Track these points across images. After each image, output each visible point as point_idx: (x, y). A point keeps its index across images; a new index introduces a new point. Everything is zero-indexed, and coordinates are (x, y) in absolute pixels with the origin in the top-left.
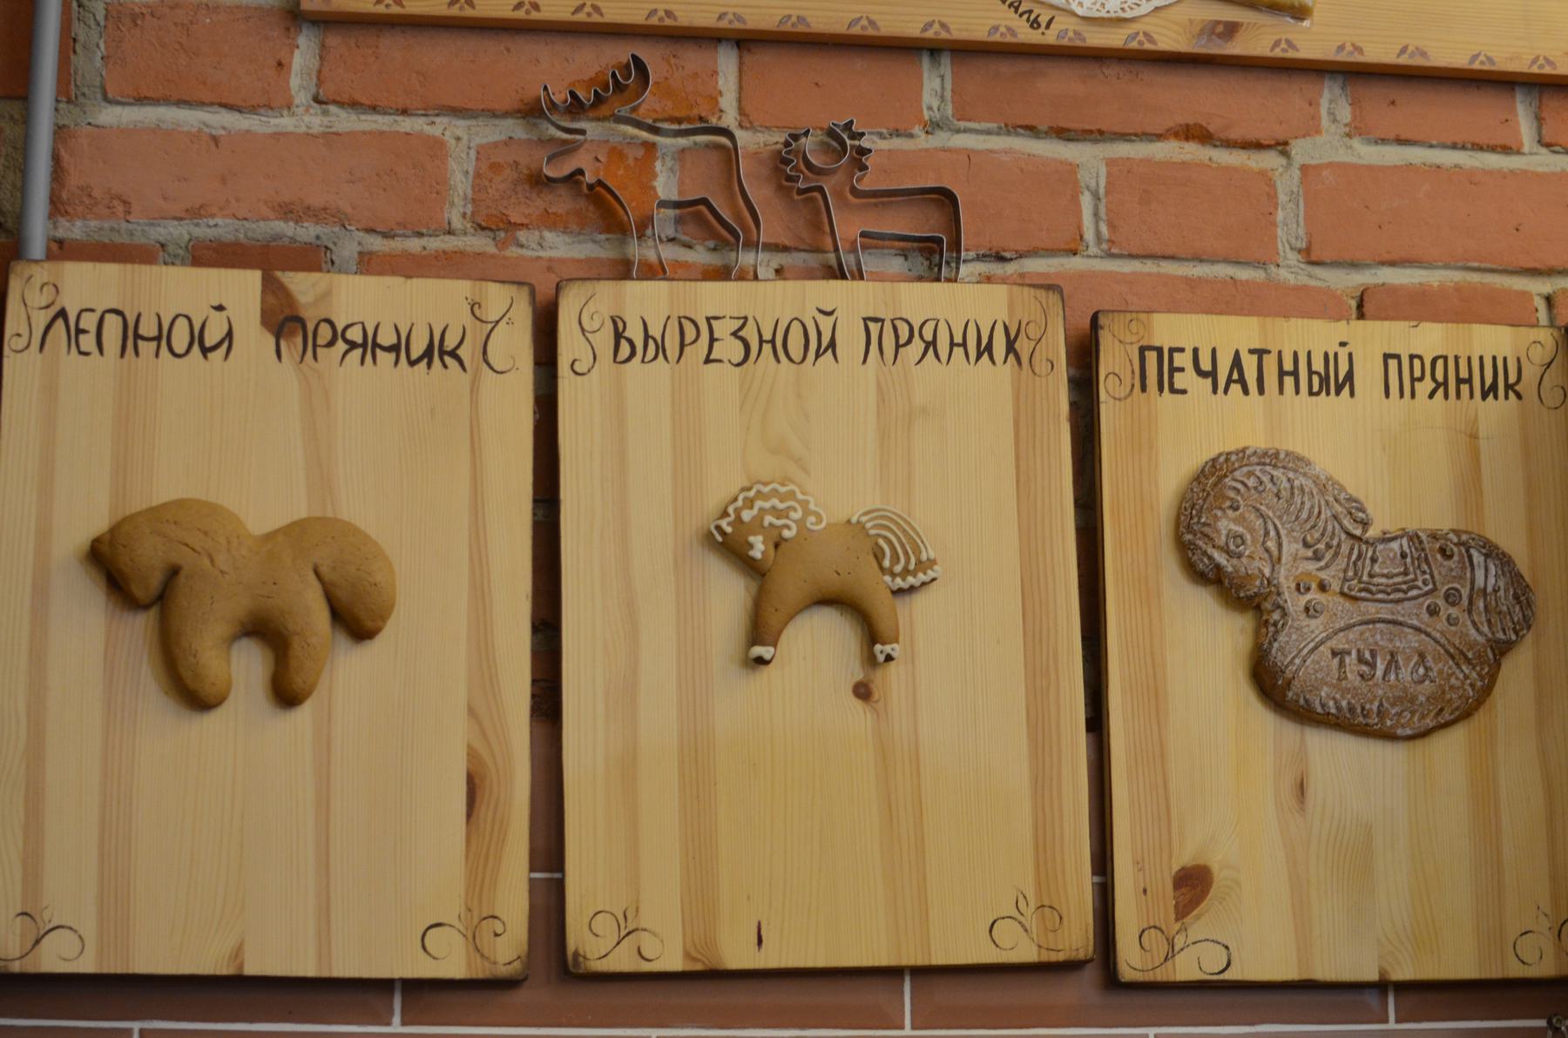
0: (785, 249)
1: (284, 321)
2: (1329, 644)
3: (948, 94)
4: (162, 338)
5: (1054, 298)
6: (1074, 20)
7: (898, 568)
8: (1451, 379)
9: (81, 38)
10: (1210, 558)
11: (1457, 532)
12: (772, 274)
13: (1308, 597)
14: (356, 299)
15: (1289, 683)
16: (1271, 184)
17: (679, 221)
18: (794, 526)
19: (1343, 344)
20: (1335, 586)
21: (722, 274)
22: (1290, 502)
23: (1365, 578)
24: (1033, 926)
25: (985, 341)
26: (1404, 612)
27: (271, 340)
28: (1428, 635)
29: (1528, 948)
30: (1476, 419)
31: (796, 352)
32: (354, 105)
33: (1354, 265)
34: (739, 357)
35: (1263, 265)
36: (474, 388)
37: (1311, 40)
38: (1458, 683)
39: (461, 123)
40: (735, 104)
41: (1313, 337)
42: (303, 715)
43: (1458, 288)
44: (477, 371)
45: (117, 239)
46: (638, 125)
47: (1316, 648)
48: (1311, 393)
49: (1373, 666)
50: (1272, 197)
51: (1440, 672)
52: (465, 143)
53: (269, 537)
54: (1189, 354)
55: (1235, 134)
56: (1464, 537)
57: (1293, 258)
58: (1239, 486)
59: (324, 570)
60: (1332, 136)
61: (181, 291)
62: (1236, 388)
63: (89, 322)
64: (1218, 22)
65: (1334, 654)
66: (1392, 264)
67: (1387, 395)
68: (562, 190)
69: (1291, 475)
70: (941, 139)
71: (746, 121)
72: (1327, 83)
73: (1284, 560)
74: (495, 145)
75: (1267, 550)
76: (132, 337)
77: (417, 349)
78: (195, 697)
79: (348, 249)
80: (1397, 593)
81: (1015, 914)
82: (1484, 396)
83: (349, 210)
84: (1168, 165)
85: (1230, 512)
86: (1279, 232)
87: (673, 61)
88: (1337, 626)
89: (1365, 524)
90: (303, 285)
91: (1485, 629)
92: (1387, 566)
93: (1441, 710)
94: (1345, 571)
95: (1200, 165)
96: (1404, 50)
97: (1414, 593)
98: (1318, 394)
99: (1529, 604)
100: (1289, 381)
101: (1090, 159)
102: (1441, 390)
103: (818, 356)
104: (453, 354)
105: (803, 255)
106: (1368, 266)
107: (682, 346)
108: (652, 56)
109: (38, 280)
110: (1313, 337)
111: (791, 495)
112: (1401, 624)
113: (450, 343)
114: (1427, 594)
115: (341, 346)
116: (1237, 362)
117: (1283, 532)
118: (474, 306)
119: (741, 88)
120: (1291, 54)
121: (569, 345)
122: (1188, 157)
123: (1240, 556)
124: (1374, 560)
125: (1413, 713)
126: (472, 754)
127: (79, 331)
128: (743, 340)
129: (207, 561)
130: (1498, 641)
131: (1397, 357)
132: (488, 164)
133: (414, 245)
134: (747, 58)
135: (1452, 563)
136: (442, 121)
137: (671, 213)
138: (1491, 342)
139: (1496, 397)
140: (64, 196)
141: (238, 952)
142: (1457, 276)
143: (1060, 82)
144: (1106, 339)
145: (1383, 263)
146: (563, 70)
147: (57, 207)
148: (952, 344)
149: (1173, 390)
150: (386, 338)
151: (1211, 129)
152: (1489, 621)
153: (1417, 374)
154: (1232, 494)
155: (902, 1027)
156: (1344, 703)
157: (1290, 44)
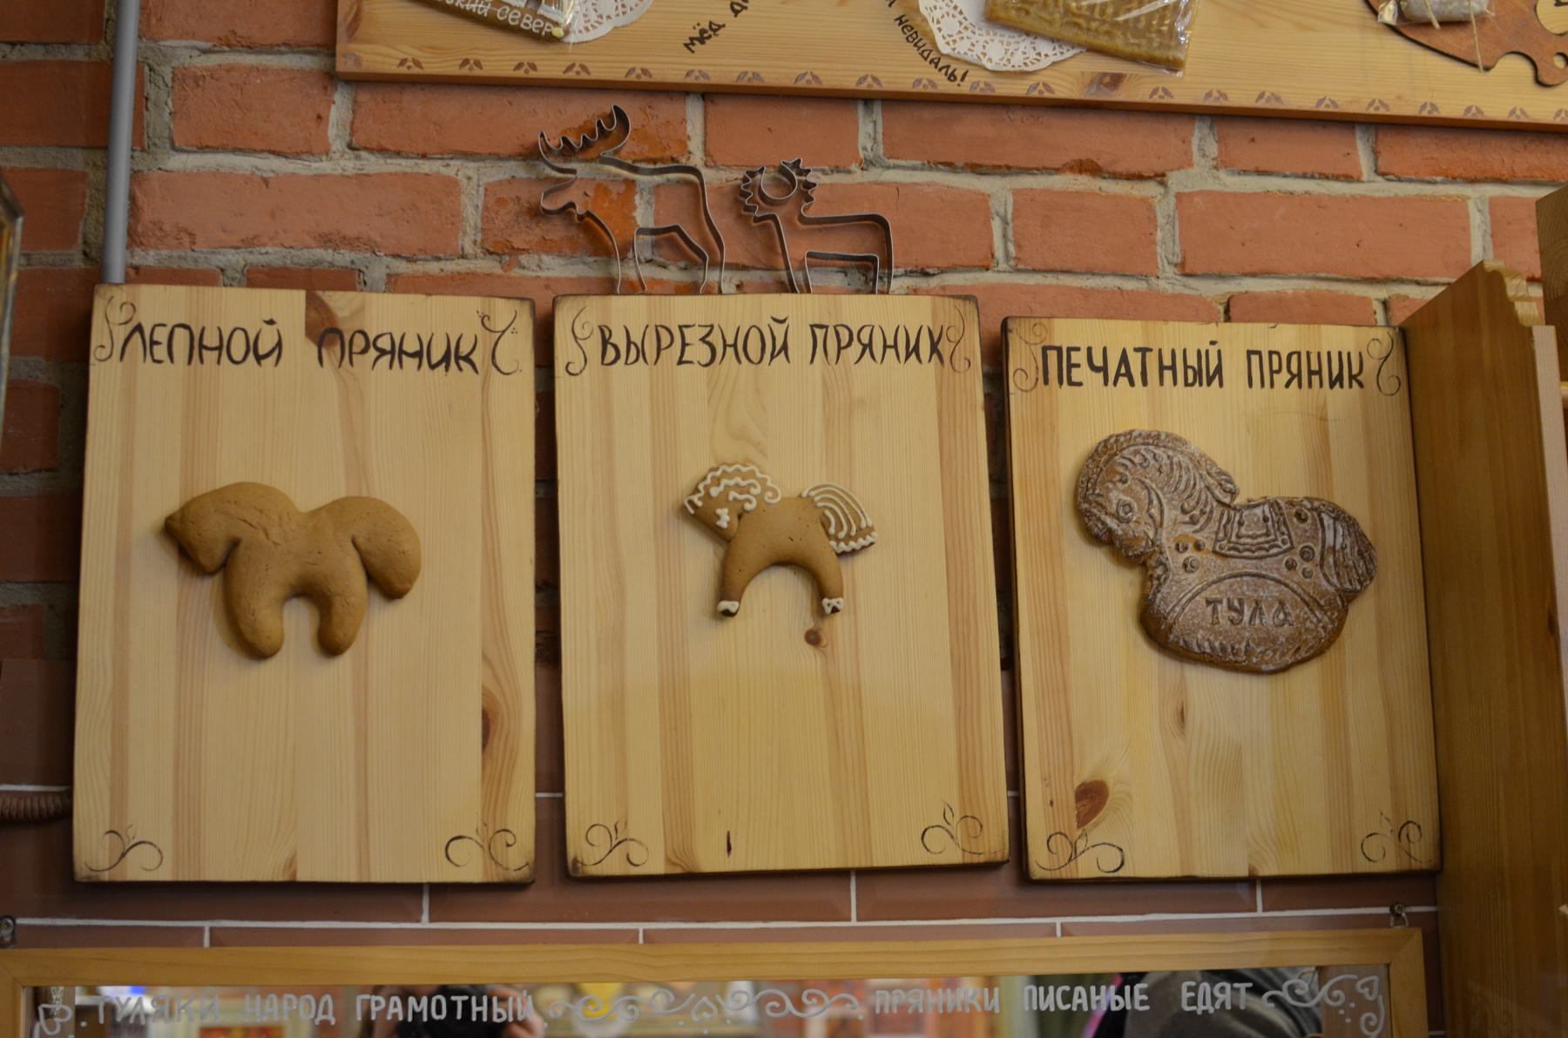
0: (744, 268)
1: (325, 333)
3: (880, 137)
4: (223, 347)
7: (842, 535)
8: (1304, 371)
9: (152, 97)
10: (1104, 523)
11: (1310, 499)
12: (733, 289)
13: (1186, 555)
14: (383, 313)
15: (1170, 628)
16: (1151, 209)
17: (655, 245)
19: (1213, 343)
20: (1209, 546)
21: (692, 289)
22: (1169, 476)
25: (912, 344)
26: (1265, 566)
27: (315, 349)
28: (1287, 586)
32: (381, 151)
33: (1221, 277)
34: (706, 358)
35: (1144, 277)
36: (485, 387)
37: (1183, 89)
39: (471, 165)
40: (701, 147)
41: (1187, 337)
42: (345, 661)
43: (1309, 295)
45: (185, 265)
46: (620, 165)
48: (1187, 384)
49: (1241, 612)
50: (1152, 220)
51: (1298, 617)
52: (474, 182)
53: (315, 513)
54: (1084, 352)
55: (1121, 168)
56: (1316, 504)
57: (1170, 271)
59: (360, 541)
60: (1201, 168)
61: (239, 308)
62: (1123, 381)
63: (161, 335)
64: (1105, 74)
65: (1208, 602)
66: (1254, 275)
67: (1251, 385)
68: (558, 221)
70: (874, 175)
72: (1197, 124)
74: (501, 183)
75: (1151, 516)
76: (197, 347)
80: (1261, 551)
81: (943, 823)
82: (1332, 386)
83: (378, 239)
84: (1065, 194)
85: (1119, 485)
89: (1233, 494)
90: (340, 303)
91: (1335, 580)
92: (1251, 529)
95: (1092, 194)
97: (1275, 550)
98: (1192, 385)
100: (1168, 374)
101: (999, 190)
103: (772, 357)
104: (467, 359)
105: (759, 273)
106: (1233, 277)
107: (659, 350)
108: (630, 106)
109: (118, 301)
110: (1187, 337)
111: (752, 474)
112: (1264, 577)
113: (464, 350)
115: (373, 353)
116: (1124, 359)
117: (1164, 501)
119: (706, 133)
121: (565, 350)
122: (1082, 188)
123: (1128, 521)
124: (1241, 524)
125: (1275, 652)
126: (487, 695)
127: (153, 343)
129: (262, 536)
130: (1345, 591)
131: (1259, 353)
132: (495, 199)
133: (434, 267)
134: (711, 108)
136: (456, 163)
137: (649, 238)
138: (1337, 339)
141: (291, 863)
142: (1308, 285)
143: (974, 125)
145: (1246, 275)
148: (885, 347)
149: (1071, 383)
150: (411, 346)
151: (1101, 163)
152: (1338, 574)
153: (1275, 367)
154: (1121, 470)
155: (849, 919)
156: (1217, 644)
157: (1166, 92)
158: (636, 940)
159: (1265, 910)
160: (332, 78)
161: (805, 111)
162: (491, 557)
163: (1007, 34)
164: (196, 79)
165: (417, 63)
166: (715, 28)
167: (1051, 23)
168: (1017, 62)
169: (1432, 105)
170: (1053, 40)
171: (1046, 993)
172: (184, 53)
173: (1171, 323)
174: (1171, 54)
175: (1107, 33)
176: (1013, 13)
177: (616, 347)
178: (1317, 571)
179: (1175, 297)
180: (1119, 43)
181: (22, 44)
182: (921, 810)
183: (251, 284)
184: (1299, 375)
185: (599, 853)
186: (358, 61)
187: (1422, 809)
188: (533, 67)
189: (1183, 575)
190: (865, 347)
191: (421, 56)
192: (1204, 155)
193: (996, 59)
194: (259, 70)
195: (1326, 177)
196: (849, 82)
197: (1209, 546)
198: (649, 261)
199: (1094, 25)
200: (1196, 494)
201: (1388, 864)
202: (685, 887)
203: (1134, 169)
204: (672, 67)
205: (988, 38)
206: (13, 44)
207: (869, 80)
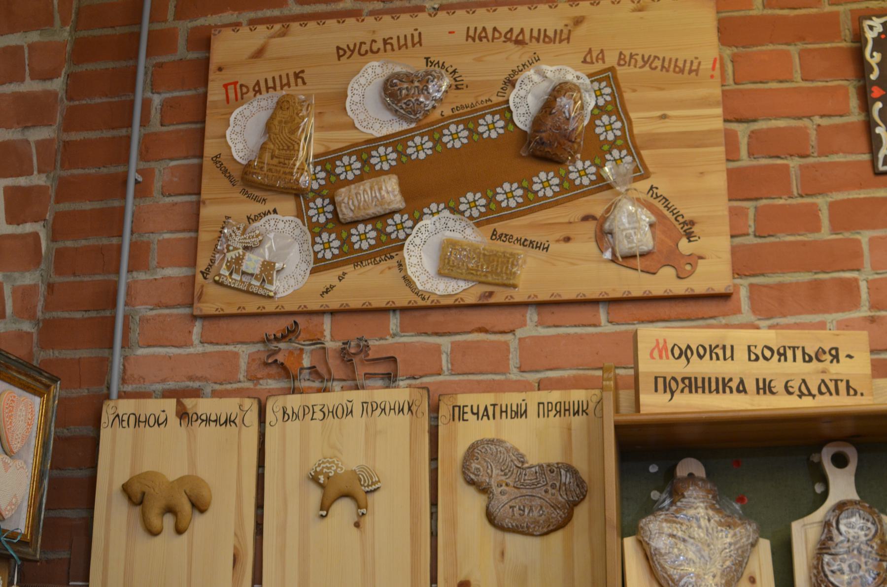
1: (183, 414)
5: (425, 392)
11: (558, 464)
12: (339, 389)
14: (204, 406)
16: (508, 345)
17: (310, 373)
20: (512, 484)
21: (325, 390)
22: (496, 456)
32: (211, 343)
33: (537, 371)
34: (321, 417)
35: (504, 373)
36: (239, 432)
37: (519, 295)
41: (512, 399)
42: (185, 536)
43: (574, 377)
49: (524, 511)
50: (508, 350)
52: (244, 352)
53: (173, 482)
54: (469, 407)
55: (496, 329)
57: (515, 371)
59: (187, 491)
60: (531, 327)
62: (485, 418)
63: (125, 418)
65: (511, 507)
66: (551, 369)
68: (274, 366)
71: (333, 339)
72: (530, 308)
74: (254, 353)
76: (138, 421)
77: (222, 421)
78: (154, 533)
79: (208, 390)
80: (534, 485)
82: (574, 415)
84: (473, 342)
89: (523, 463)
91: (565, 497)
92: (528, 478)
99: (583, 487)
100: (504, 414)
101: (445, 342)
104: (233, 422)
108: (299, 320)
109: (111, 406)
110: (512, 399)
111: (333, 462)
113: (232, 419)
115: (199, 421)
116: (486, 409)
120: (512, 300)
126: (235, 548)
132: (252, 358)
133: (229, 387)
135: (554, 475)
137: (308, 371)
138: (578, 395)
143: (435, 317)
146: (276, 326)
147: (124, 381)
149: (463, 420)
150: (213, 418)
157: (511, 297)
160: (194, 317)
161: (369, 316)
162: (239, 497)
164: (148, 320)
166: (332, 287)
168: (450, 291)
172: (144, 311)
173: (506, 394)
174: (511, 282)
175: (485, 276)
178: (557, 494)
179: (516, 381)
180: (490, 279)
186: (201, 310)
188: (264, 308)
189: (500, 496)
191: (223, 306)
194: (170, 315)
197: (512, 484)
203: (502, 329)
204: (314, 306)
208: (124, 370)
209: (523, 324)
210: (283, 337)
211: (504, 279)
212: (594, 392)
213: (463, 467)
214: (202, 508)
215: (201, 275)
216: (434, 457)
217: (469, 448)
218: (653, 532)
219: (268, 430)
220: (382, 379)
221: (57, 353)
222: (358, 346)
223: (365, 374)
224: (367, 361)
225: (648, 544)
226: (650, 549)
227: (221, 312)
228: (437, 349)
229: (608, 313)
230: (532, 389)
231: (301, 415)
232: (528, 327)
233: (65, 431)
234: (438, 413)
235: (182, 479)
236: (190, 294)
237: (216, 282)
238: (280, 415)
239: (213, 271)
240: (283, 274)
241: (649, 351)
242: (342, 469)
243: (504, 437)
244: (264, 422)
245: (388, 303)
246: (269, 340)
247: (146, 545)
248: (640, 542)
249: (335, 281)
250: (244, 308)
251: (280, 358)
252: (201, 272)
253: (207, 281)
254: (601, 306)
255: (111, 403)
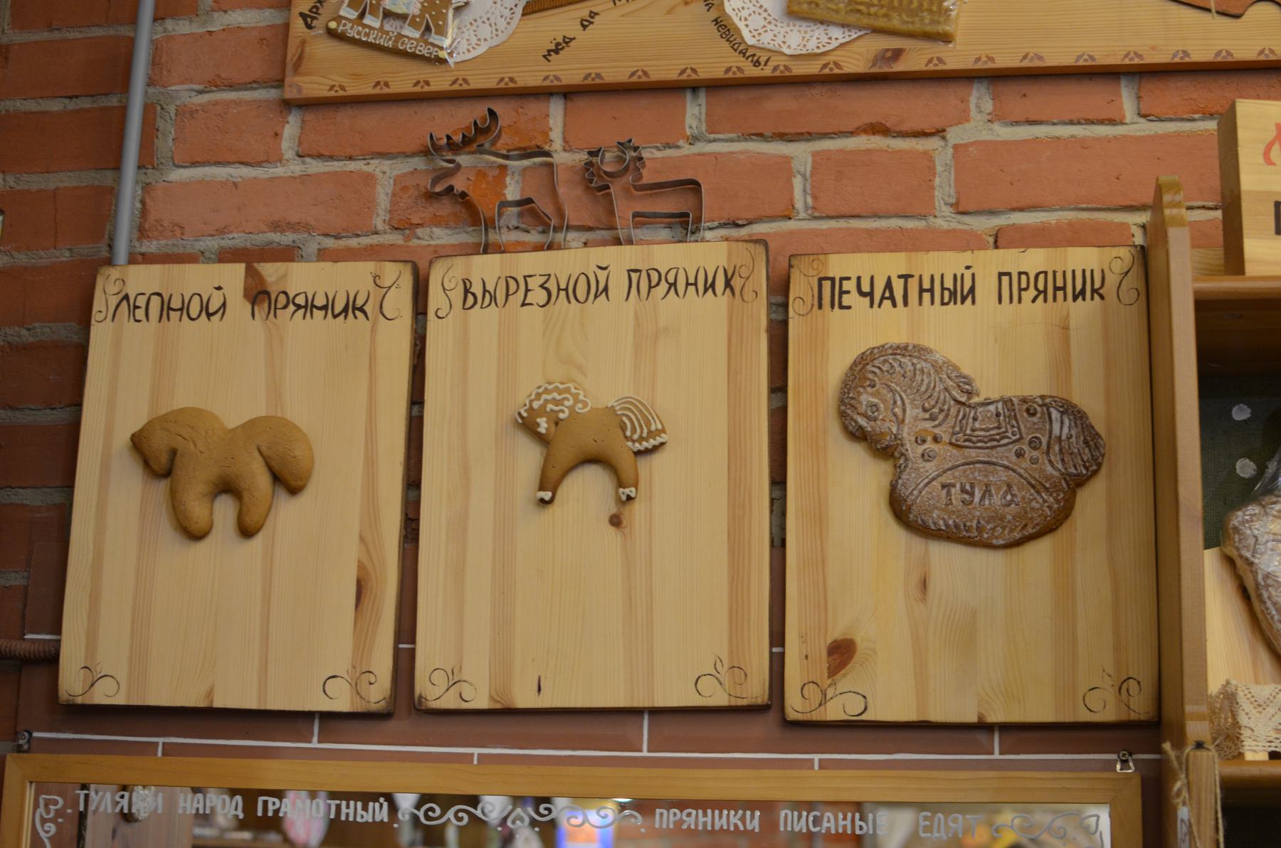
0: (590, 229)
1: (258, 294)
2: (940, 479)
3: (703, 117)
4: (184, 309)
5: (760, 249)
6: (784, 58)
7: (636, 437)
8: (1049, 288)
9: (161, 129)
10: (856, 422)
11: (1042, 397)
13: (925, 446)
14: (302, 278)
15: (909, 508)
17: (520, 215)
18: (567, 411)
19: (968, 268)
20: (946, 438)
22: (912, 380)
23: (968, 432)
24: (726, 680)
25: (710, 280)
26: (994, 456)
27: (249, 306)
28: (1014, 471)
29: (1094, 700)
30: (1068, 315)
31: (581, 296)
32: (320, 156)
33: (992, 212)
35: (923, 217)
36: (373, 330)
37: (955, 58)
38: (1037, 506)
39: (388, 162)
40: (561, 135)
42: (258, 542)
43: (1071, 224)
44: (376, 319)
45: (176, 250)
46: (497, 155)
47: (929, 483)
48: (943, 304)
49: (972, 494)
50: (932, 169)
51: (1023, 498)
52: (386, 173)
53: (234, 430)
55: (906, 127)
56: (1048, 401)
57: (947, 211)
58: (877, 370)
59: (264, 449)
60: (979, 122)
61: (195, 279)
62: (887, 303)
63: (141, 301)
64: (887, 50)
65: (943, 486)
66: (1022, 209)
68: (446, 200)
69: (915, 361)
70: (701, 147)
71: (567, 148)
72: (976, 85)
73: (907, 421)
74: (405, 175)
75: (895, 415)
76: (166, 308)
77: (339, 307)
78: (194, 534)
80: (993, 442)
81: (714, 672)
82: (1075, 298)
83: (313, 223)
85: (869, 389)
86: (937, 193)
87: (520, 110)
88: (946, 467)
89: (969, 394)
90: (270, 271)
91: (1060, 466)
92: (983, 424)
93: (1026, 525)
94: (953, 427)
95: (882, 151)
96: (1025, 57)
97: (1006, 441)
98: (947, 304)
99: (1097, 448)
100: (926, 296)
101: (801, 154)
102: (1042, 296)
103: (596, 297)
104: (361, 309)
105: (603, 232)
106: (1002, 213)
107: (507, 295)
108: (500, 107)
109: (113, 278)
112: (994, 464)
113: (359, 303)
114: (1014, 442)
115: (292, 308)
116: (889, 285)
117: (907, 402)
118: (376, 277)
119: (565, 125)
121: (436, 299)
122: (871, 146)
124: (975, 419)
125: (1004, 528)
126: (361, 567)
127: (136, 307)
128: (546, 289)
129: (192, 446)
130: (1070, 475)
131: (1009, 274)
132: (401, 186)
133: (353, 242)
134: (570, 104)
135: (1035, 419)
137: (515, 210)
138: (1082, 259)
139: (1084, 299)
140: (147, 226)
141: (210, 693)
143: (780, 102)
144: (795, 275)
145: (1014, 210)
147: (142, 232)
148: (688, 284)
149: (841, 307)
151: (888, 124)
152: (1063, 460)
153: (1024, 285)
154: (871, 376)
155: (641, 751)
156: (951, 522)
157: (940, 60)
158: (812, 767)
159: (649, 751)
160: (288, 105)
161: (643, 102)
163: (804, 24)
164: (193, 113)
165: (343, 88)
166: (567, 41)
167: (837, 12)
168: (812, 46)
169: (1184, 52)
170: (843, 26)
171: (800, 817)
172: (185, 94)
175: (885, 15)
176: (805, 6)
177: (474, 294)
179: (948, 231)
180: (896, 23)
181: (77, 97)
182: (693, 659)
183: (221, 261)
184: (1045, 291)
185: (437, 691)
186: (300, 89)
187: (1142, 668)
188: (427, 83)
189: (921, 463)
190: (670, 285)
192: (981, 112)
193: (794, 46)
195: (1092, 123)
196: (673, 75)
197: (946, 438)
198: (517, 228)
199: (873, 10)
200: (935, 395)
201: (1108, 714)
202: (504, 718)
204: (530, 77)
205: (788, 29)
206: (71, 98)
207: (689, 71)
208: (144, 212)
209: (964, 118)
210: (467, 141)
211: (925, 23)
212: (1116, 251)
213: (842, 402)
214: (294, 483)
215: (300, 21)
216: (779, 386)
217: (855, 364)
218: (1262, 540)
219: (432, 324)
220: (670, 226)
221: (11, 180)
222: (621, 160)
223: (636, 215)
224: (636, 188)
225: (1251, 564)
226: (1255, 573)
227: (341, 93)
228: (784, 167)
229: (1139, 98)
230: (982, 246)
231: (501, 296)
232: (972, 124)
233: (24, 332)
234: (787, 296)
235: (252, 423)
236: (279, 57)
237: (331, 33)
238: (457, 295)
239: (325, 12)
240: (467, 16)
241: (1262, 147)
242: (585, 404)
243: (927, 342)
244: (425, 313)
245: (683, 71)
246: (437, 148)
247: (179, 559)
248: (1230, 562)
249: (574, 30)
250: (386, 84)
251: (459, 183)
252: (302, 15)
253: (313, 33)
254: (1123, 83)
255: (114, 273)
